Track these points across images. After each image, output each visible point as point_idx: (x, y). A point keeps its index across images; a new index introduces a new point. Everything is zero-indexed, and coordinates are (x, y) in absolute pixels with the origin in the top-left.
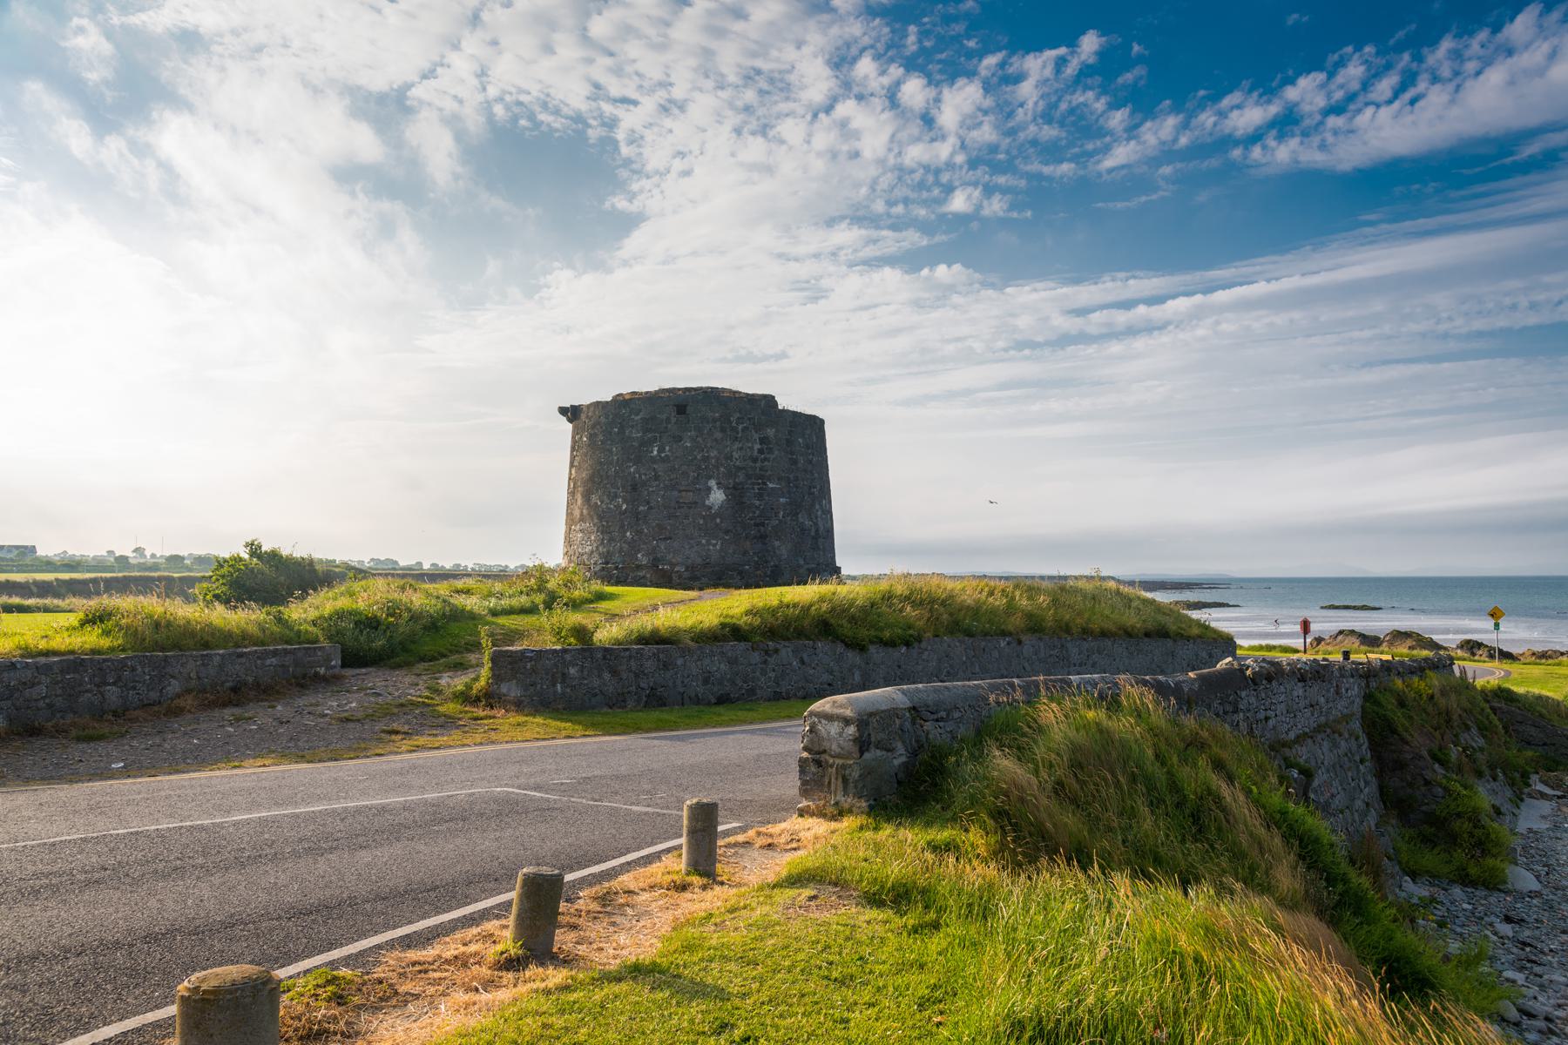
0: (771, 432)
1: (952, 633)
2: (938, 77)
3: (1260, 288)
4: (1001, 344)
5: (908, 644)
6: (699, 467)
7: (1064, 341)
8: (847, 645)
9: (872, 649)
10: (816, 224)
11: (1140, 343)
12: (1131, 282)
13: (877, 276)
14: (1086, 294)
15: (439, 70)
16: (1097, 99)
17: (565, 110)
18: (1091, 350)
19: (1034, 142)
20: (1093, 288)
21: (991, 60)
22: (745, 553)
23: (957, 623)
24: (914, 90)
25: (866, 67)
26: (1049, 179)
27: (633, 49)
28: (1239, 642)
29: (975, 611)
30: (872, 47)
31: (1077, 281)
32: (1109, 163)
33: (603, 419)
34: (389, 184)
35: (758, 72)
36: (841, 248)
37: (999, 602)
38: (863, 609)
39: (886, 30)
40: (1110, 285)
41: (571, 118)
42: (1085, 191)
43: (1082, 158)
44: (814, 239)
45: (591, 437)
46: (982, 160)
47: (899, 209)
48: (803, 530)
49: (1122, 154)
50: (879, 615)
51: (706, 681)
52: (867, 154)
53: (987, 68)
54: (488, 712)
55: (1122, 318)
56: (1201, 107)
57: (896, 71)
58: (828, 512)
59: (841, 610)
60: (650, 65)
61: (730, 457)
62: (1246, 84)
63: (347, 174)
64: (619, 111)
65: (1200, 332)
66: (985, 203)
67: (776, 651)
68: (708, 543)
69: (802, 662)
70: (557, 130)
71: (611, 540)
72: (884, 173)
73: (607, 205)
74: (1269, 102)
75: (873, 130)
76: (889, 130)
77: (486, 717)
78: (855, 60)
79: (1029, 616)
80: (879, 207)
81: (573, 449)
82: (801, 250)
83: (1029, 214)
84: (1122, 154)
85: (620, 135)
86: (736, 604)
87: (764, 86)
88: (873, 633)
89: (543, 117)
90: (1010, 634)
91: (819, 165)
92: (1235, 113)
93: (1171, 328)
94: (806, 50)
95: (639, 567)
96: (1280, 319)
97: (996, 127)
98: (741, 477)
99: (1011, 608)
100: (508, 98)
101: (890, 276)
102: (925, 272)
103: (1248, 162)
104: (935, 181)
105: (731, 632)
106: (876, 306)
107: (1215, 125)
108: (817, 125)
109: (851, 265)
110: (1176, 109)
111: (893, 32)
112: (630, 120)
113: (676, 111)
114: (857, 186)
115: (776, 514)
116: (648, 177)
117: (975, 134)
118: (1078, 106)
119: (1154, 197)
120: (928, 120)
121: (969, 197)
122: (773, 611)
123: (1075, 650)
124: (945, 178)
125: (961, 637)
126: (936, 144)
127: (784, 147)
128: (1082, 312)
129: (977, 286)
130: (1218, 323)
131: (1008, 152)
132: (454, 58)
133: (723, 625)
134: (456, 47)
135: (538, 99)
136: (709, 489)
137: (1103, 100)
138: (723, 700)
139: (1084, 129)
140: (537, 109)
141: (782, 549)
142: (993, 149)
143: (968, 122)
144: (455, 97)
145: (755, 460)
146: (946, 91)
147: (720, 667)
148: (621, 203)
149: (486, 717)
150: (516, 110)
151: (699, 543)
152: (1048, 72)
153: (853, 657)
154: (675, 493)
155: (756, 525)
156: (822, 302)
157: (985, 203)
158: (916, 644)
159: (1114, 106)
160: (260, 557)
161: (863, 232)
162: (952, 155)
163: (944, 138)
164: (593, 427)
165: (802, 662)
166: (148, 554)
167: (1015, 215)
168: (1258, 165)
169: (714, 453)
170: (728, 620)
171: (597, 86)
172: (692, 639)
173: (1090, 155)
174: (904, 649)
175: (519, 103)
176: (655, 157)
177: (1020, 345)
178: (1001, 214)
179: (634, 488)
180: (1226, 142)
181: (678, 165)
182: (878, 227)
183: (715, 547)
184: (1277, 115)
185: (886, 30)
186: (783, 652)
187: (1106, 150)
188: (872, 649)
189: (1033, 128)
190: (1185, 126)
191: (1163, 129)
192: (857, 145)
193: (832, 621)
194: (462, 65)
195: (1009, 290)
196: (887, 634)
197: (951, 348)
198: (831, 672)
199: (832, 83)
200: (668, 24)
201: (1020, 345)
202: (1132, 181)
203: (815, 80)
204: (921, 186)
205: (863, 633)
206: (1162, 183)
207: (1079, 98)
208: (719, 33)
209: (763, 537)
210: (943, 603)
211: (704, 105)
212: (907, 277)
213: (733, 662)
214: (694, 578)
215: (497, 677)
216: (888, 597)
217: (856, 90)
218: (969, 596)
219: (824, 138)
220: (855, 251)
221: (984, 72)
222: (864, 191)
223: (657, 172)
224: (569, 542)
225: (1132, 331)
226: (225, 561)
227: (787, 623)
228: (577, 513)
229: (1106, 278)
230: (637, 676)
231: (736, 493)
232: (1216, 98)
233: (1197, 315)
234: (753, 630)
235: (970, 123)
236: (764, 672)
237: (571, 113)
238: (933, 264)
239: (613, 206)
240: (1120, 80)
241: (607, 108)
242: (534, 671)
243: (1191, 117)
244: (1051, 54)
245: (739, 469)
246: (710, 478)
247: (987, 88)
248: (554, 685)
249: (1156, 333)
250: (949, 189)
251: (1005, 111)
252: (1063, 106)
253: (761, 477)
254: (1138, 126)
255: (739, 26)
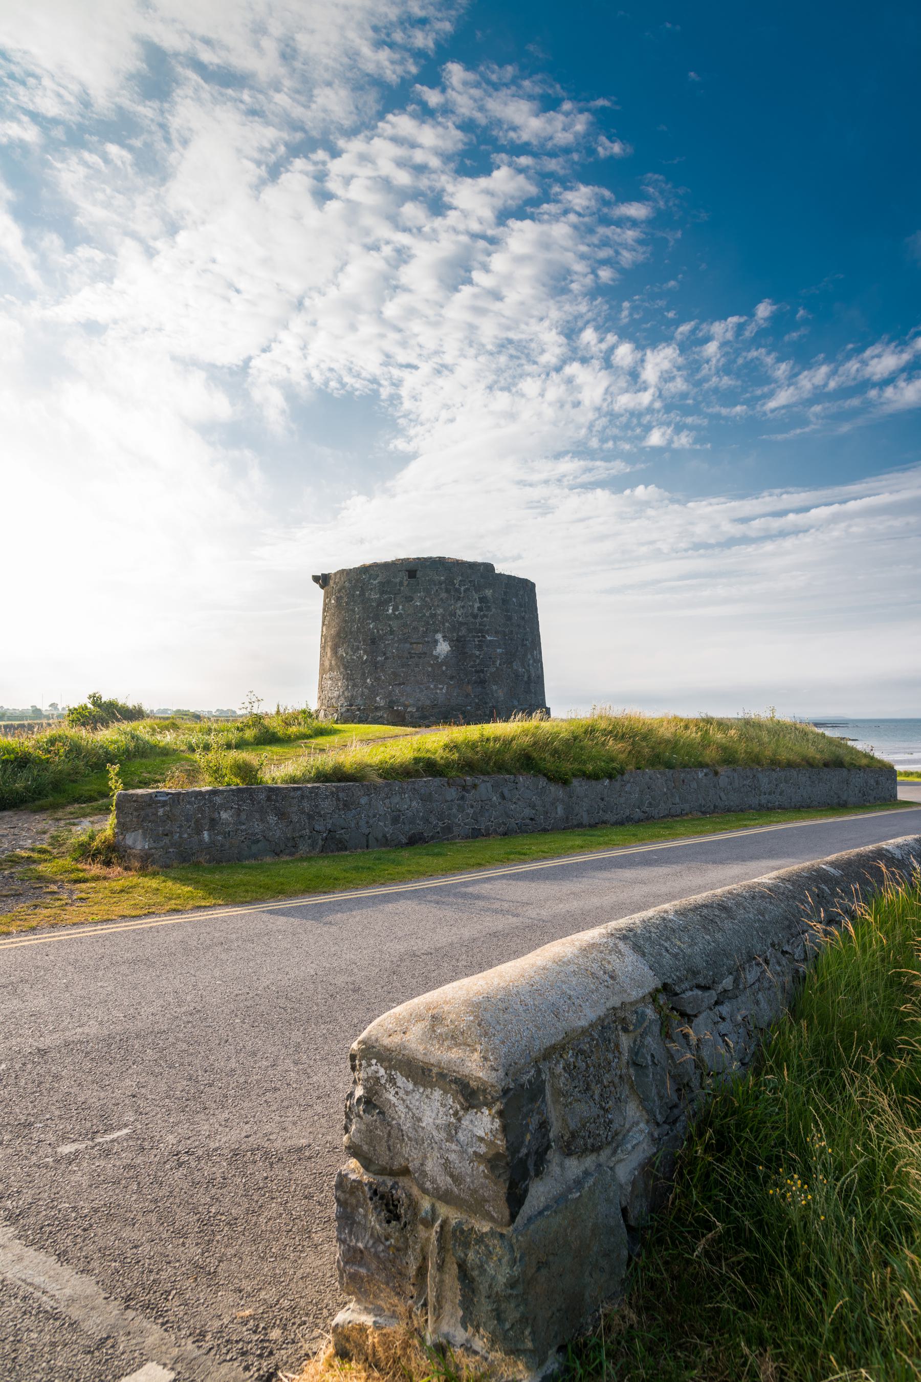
0: (489, 593)
1: (653, 765)
2: (644, 343)
3: (885, 498)
4: (682, 545)
5: (611, 777)
6: (428, 623)
7: (731, 542)
8: (549, 779)
9: (575, 782)
10: (546, 457)
11: (789, 543)
12: (785, 496)
13: (590, 496)
14: (748, 506)
15: (273, 345)
16: (769, 353)
17: (364, 374)
18: (750, 549)
19: (716, 390)
20: (755, 501)
21: (685, 328)
22: (467, 695)
23: (658, 756)
24: (624, 353)
25: (589, 336)
26: (726, 418)
27: (416, 326)
28: (898, 768)
29: (674, 744)
30: (594, 320)
31: (742, 497)
32: (772, 404)
33: (347, 584)
34: (236, 436)
35: (510, 341)
36: (565, 476)
37: (694, 735)
38: (566, 742)
39: (606, 307)
40: (768, 499)
41: (369, 381)
42: (755, 426)
43: (751, 402)
44: (547, 469)
45: (338, 599)
46: (674, 406)
47: (610, 444)
48: (517, 676)
49: (783, 397)
50: (582, 748)
51: (395, 820)
52: (587, 402)
53: (681, 333)
54: (105, 871)
55: (776, 524)
56: (848, 358)
57: (611, 338)
58: (539, 661)
59: (542, 744)
60: (426, 336)
61: (453, 614)
62: (885, 337)
63: (207, 430)
64: (406, 374)
65: (836, 534)
66: (675, 438)
67: (475, 786)
68: (436, 688)
69: (503, 797)
70: (357, 390)
71: (354, 686)
72: (600, 417)
73: (391, 446)
74: (902, 352)
75: (592, 385)
76: (605, 383)
77: (96, 879)
78: (581, 330)
79: (724, 748)
80: (594, 443)
81: (324, 610)
82: (536, 477)
83: (709, 446)
84: (783, 397)
85: (404, 392)
86: (435, 740)
87: (512, 351)
88: (576, 766)
89: (348, 379)
90: (707, 766)
91: (549, 413)
92: (876, 360)
93: (813, 531)
94: (546, 323)
95: (377, 709)
96: (898, 523)
97: (687, 380)
98: (464, 631)
99: (706, 741)
100: (323, 366)
101: (601, 496)
102: (628, 492)
103: (882, 400)
104: (636, 423)
105: (427, 767)
106: (589, 518)
107: (857, 370)
108: (549, 382)
109: (572, 488)
110: (828, 360)
111: (611, 308)
112: (411, 380)
113: (446, 372)
114: (579, 427)
115: (494, 662)
116: (422, 424)
117: (671, 385)
118: (752, 360)
119: (807, 430)
120: (634, 375)
121: (664, 434)
122: (473, 746)
123: (766, 780)
124: (646, 419)
125: (662, 769)
126: (640, 394)
127: (523, 400)
128: (745, 520)
129: (667, 502)
130: (849, 526)
131: (694, 399)
132: (283, 335)
133: (417, 760)
134: (286, 327)
135: (345, 366)
136: (436, 642)
137: (773, 355)
138: (415, 841)
139: (755, 378)
140: (344, 373)
141: (499, 692)
142: (684, 396)
143: (666, 376)
144: (286, 366)
145: (475, 617)
146: (649, 352)
147: (411, 805)
148: (400, 444)
149: (96, 879)
150: (328, 374)
151: (428, 688)
152: (729, 336)
153: (556, 791)
154: (408, 645)
155: (477, 672)
156: (549, 516)
157: (675, 438)
158: (619, 777)
159: (779, 360)
160: (99, 706)
161: (582, 463)
162: (652, 402)
163: (645, 389)
164: (340, 591)
165: (503, 797)
166: (60, 707)
167: (698, 447)
168: (889, 402)
169: (440, 611)
170: (423, 755)
171: (388, 356)
172: (380, 776)
173: (759, 398)
174: (607, 782)
175: (331, 370)
176: (427, 408)
177: (697, 547)
178: (688, 446)
179: (373, 642)
180: (864, 385)
181: (444, 415)
182: (593, 459)
183: (442, 691)
184: (908, 363)
185: (606, 307)
186: (482, 788)
187: (771, 395)
188: (575, 782)
189: (715, 379)
190: (834, 373)
191: (818, 375)
192: (580, 397)
193: (535, 755)
194: (289, 341)
195: (691, 505)
196: (590, 767)
197: (644, 549)
198: (533, 807)
199: (564, 349)
200: (442, 307)
201: (697, 547)
202: (793, 416)
203: (552, 344)
204: (627, 426)
205: (567, 767)
206: (813, 419)
207: (754, 354)
208: (480, 311)
209: (482, 682)
210: (645, 738)
211: (467, 367)
212: (613, 497)
213: (426, 799)
214: (424, 718)
215: (122, 827)
216: (590, 731)
217: (580, 354)
218: (666, 732)
219: (555, 391)
220: (575, 477)
221: (678, 336)
222: (583, 431)
223: (428, 420)
224: (321, 689)
225: (783, 534)
226: (75, 709)
227: (487, 757)
228: (327, 663)
229: (765, 494)
230: (310, 817)
231: (459, 645)
232: (860, 350)
233: (835, 519)
234: (449, 765)
235: (666, 378)
236: (461, 809)
237: (368, 377)
238: (633, 486)
239: (395, 447)
240: (786, 338)
241: (396, 373)
242: (168, 817)
243: (839, 366)
244: (733, 320)
245: (461, 624)
246: (437, 631)
247: (683, 348)
248: (199, 832)
249: (801, 535)
250: (648, 429)
251: (692, 368)
252: (740, 361)
253: (481, 631)
254: (796, 375)
255: (497, 306)
